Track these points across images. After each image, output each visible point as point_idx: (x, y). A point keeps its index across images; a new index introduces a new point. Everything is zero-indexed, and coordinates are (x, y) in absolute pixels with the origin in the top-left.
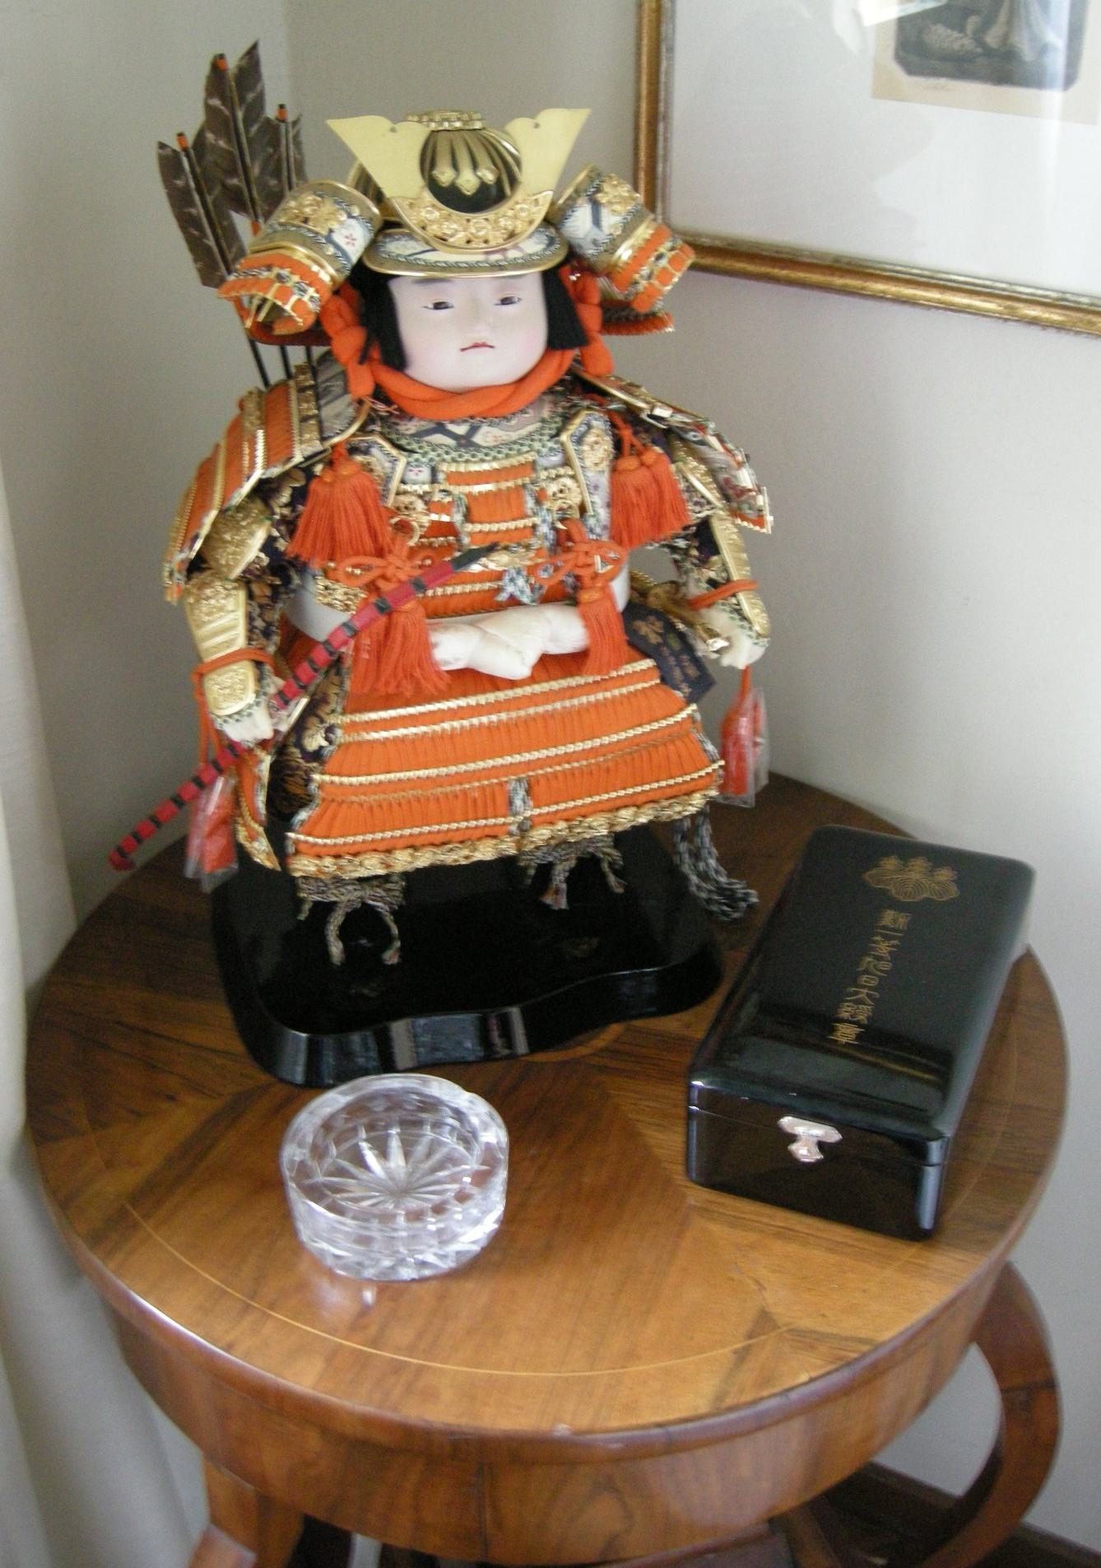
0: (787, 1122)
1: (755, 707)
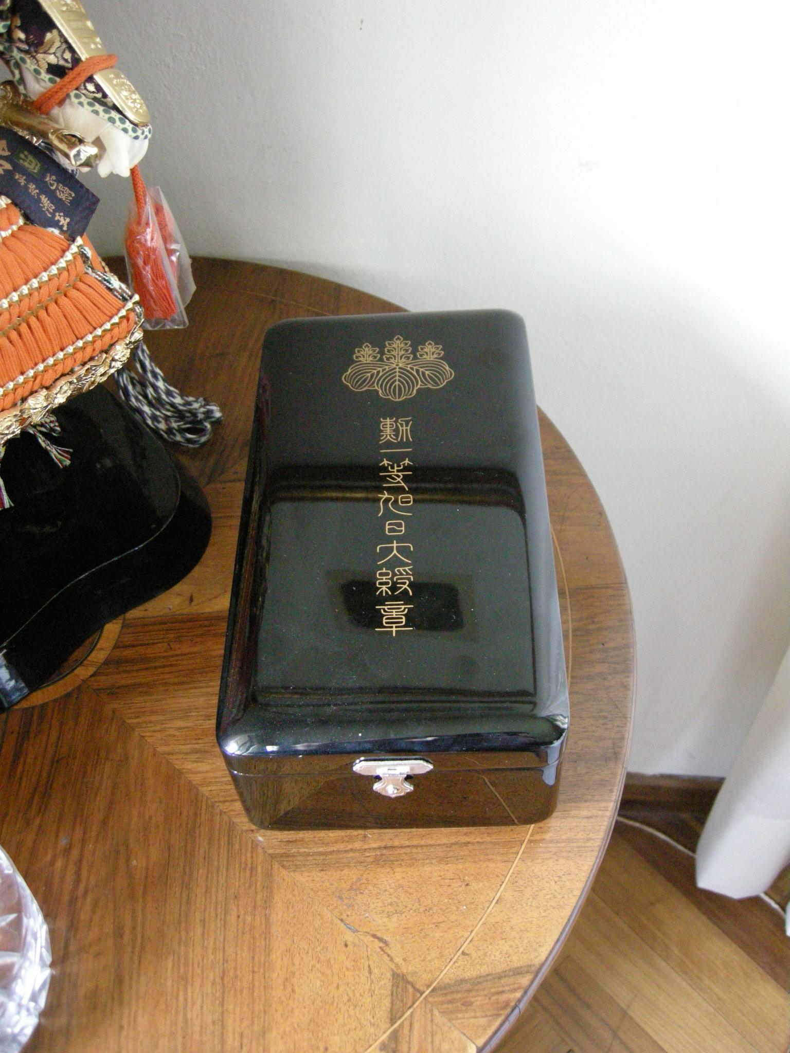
0: (361, 766)
1: (158, 210)
